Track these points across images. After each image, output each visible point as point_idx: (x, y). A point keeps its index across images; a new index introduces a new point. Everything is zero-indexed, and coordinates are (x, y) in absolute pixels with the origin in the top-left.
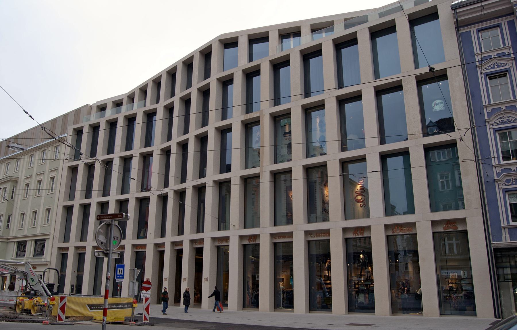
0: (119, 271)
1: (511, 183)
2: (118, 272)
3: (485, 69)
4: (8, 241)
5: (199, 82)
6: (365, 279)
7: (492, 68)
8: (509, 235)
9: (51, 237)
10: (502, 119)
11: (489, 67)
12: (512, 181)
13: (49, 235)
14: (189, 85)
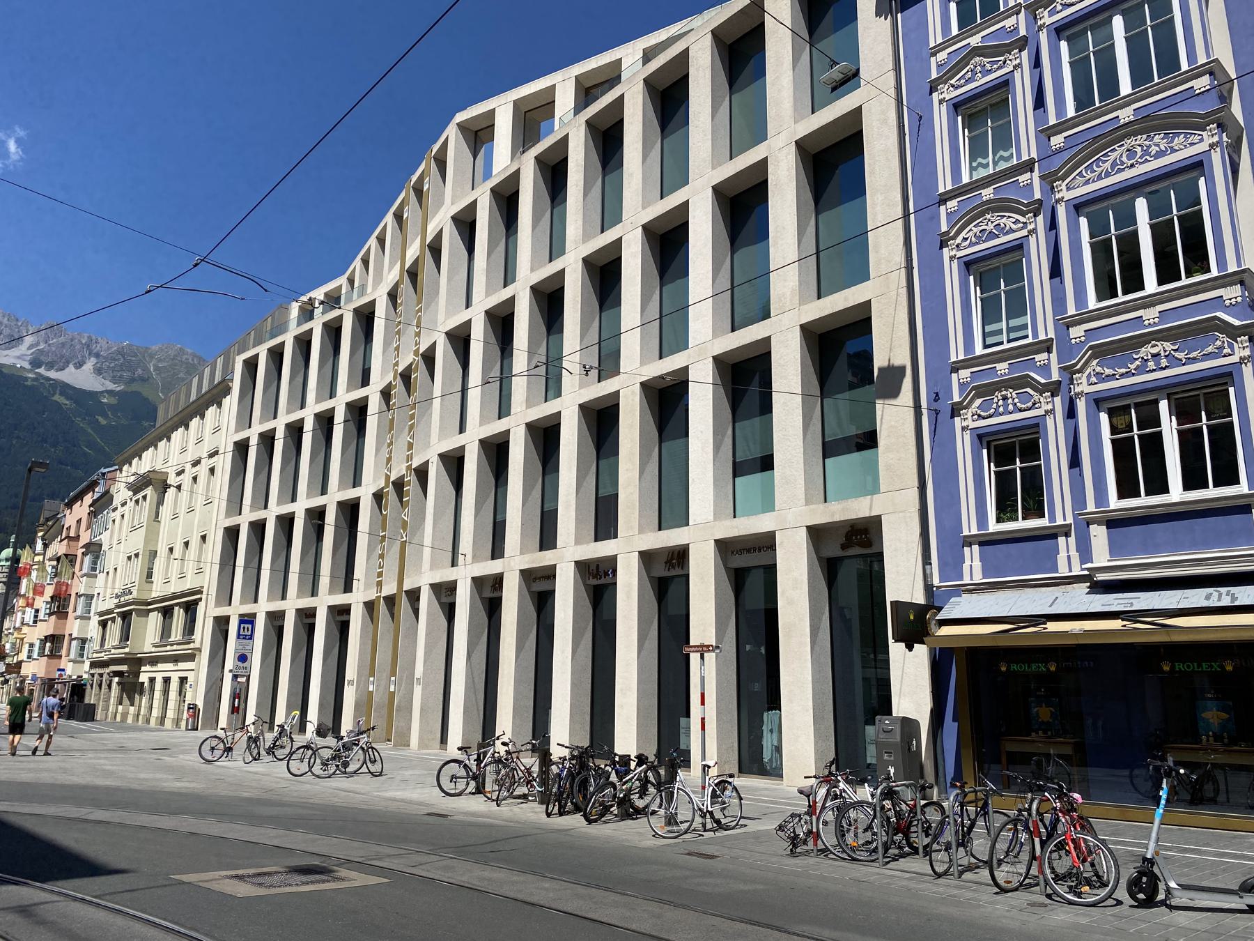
0: (244, 628)
1: (993, 411)
3: (951, 89)
4: (149, 607)
5: (586, 237)
7: (968, 81)
8: (980, 561)
9: (204, 596)
10: (981, 228)
11: (961, 82)
12: (995, 405)
13: (200, 592)
14: (555, 247)
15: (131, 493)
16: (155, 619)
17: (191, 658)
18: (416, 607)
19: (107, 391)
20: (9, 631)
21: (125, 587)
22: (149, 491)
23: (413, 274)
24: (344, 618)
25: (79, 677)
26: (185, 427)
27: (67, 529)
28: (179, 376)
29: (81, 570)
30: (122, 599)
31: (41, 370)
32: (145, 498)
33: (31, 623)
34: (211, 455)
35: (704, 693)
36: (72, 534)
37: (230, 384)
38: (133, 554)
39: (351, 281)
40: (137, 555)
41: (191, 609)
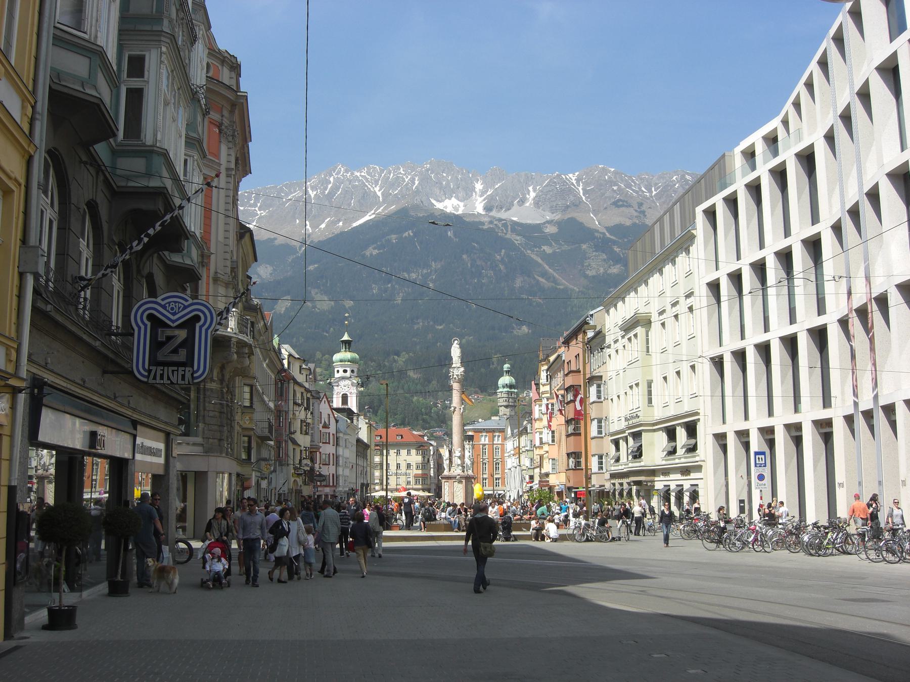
0: (759, 458)
2: (757, 459)
6: (544, 532)
9: (701, 417)
15: (623, 333)
16: (661, 439)
17: (698, 468)
18: (893, 419)
19: (548, 222)
20: (526, 448)
21: (632, 412)
22: (639, 330)
23: (846, 117)
24: (827, 430)
25: (601, 486)
26: (660, 273)
27: (568, 363)
28: (606, 195)
29: (163, 300)
30: (630, 422)
31: (494, 213)
32: (636, 336)
33: (551, 443)
34: (688, 296)
35: (748, 475)
36: (573, 368)
37: (694, 232)
38: (633, 384)
39: (785, 123)
40: (637, 385)
41: (691, 429)
